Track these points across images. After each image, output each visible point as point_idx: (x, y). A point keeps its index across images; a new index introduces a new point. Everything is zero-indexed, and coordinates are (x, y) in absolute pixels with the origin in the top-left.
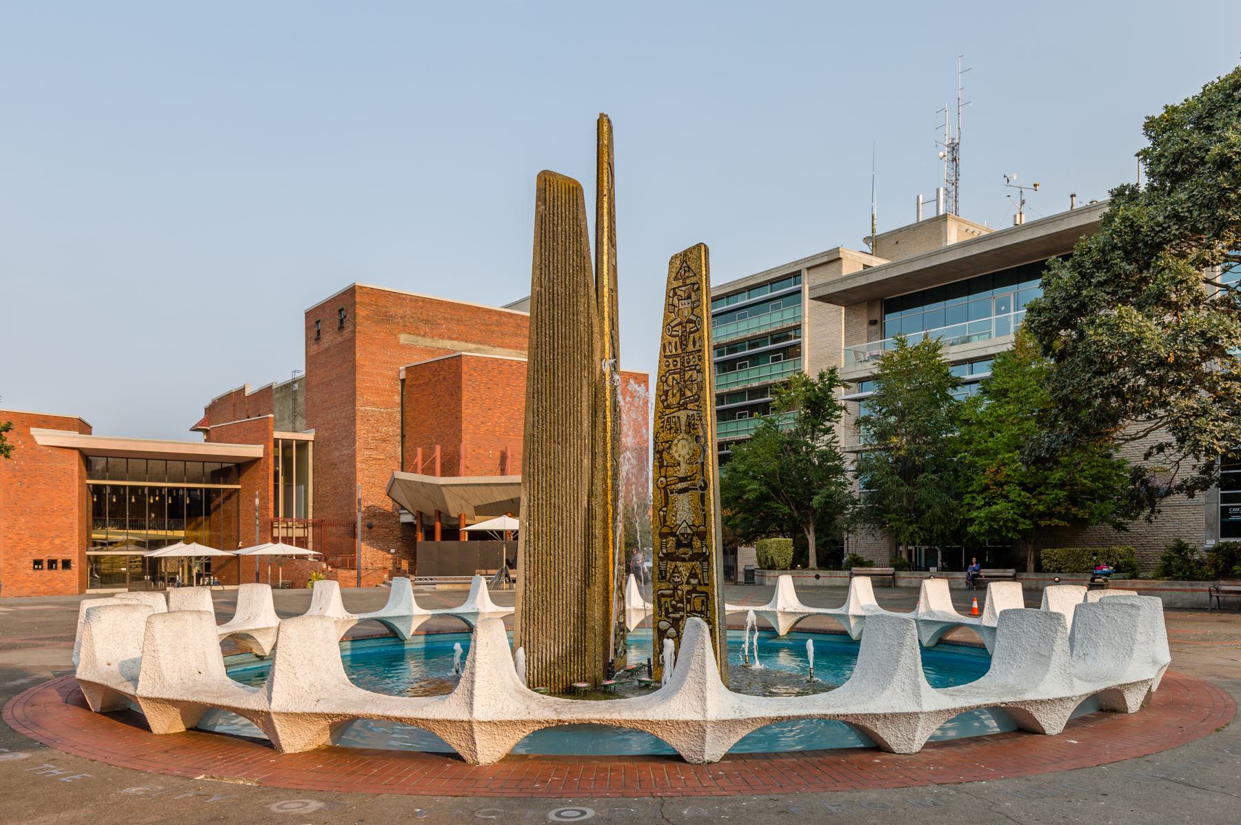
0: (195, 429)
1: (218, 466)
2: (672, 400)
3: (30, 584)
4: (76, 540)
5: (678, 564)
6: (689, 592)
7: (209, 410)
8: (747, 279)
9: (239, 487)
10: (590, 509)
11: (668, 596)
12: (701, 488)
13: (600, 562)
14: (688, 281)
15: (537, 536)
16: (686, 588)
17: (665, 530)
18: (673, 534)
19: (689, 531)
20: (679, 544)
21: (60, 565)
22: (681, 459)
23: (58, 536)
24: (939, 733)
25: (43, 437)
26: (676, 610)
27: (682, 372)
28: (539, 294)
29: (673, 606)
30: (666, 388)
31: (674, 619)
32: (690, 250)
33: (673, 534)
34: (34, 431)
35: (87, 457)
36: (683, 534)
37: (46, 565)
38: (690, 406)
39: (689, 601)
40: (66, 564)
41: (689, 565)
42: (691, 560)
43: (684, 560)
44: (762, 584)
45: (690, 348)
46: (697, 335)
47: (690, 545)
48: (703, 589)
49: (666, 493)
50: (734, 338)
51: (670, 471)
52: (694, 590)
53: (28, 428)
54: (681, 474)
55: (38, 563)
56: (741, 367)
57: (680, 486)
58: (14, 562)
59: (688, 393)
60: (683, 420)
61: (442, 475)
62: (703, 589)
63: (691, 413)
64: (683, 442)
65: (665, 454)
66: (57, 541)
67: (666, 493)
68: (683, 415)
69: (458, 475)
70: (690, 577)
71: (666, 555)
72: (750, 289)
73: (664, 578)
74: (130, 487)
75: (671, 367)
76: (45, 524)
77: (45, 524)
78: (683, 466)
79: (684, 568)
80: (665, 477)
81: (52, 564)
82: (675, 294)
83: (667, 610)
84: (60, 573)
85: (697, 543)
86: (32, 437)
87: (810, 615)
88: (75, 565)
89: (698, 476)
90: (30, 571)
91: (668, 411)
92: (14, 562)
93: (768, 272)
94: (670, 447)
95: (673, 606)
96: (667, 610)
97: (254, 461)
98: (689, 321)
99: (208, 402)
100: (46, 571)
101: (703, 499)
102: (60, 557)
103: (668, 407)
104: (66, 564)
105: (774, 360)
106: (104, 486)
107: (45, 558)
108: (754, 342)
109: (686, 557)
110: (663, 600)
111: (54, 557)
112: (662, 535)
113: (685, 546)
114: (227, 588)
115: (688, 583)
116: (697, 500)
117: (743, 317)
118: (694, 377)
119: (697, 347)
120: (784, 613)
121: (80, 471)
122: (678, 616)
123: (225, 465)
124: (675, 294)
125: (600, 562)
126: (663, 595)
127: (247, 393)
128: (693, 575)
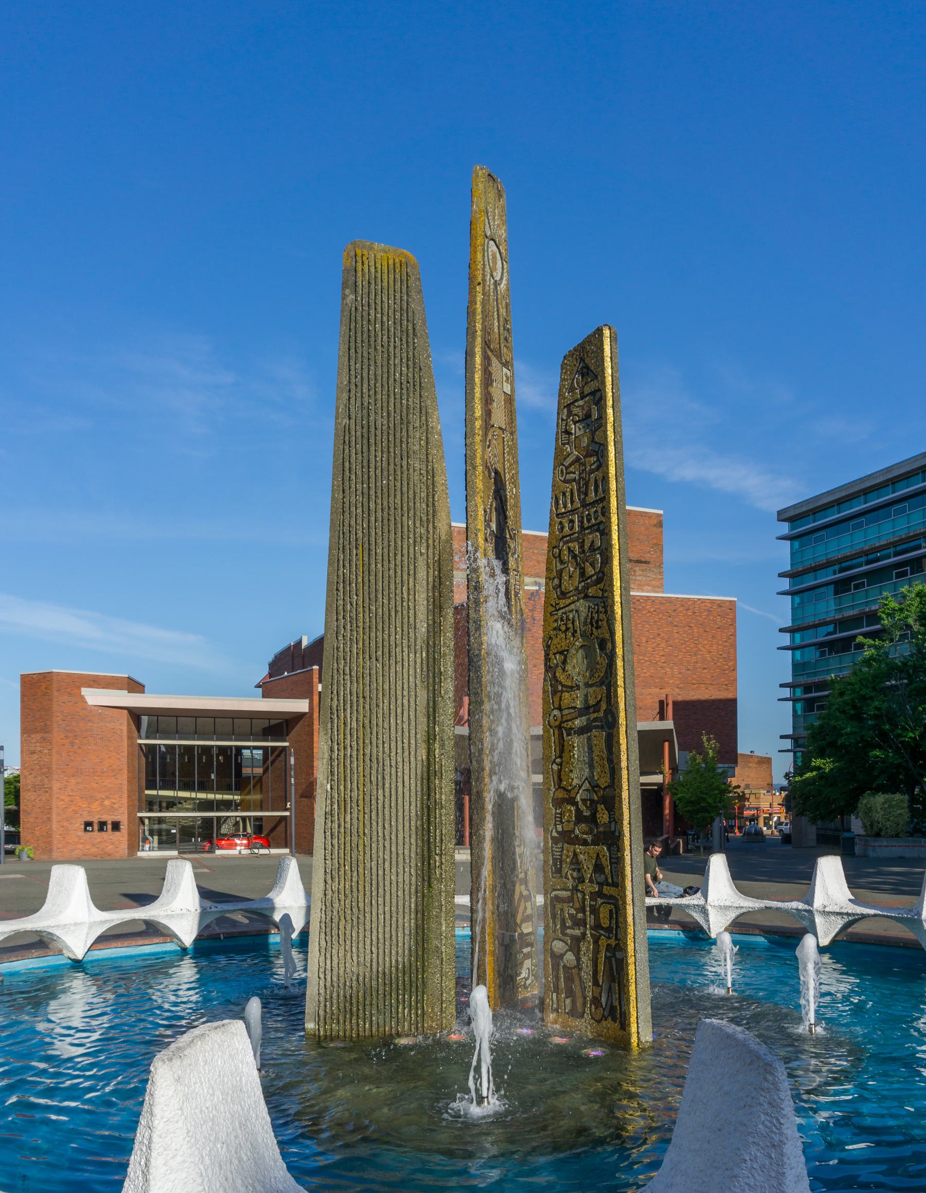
0: (256, 687)
1: (266, 723)
2: (569, 585)
3: (81, 846)
4: (125, 801)
5: (579, 848)
7: (272, 665)
8: (862, 480)
9: (286, 744)
15: (343, 804)
21: (110, 827)
23: (107, 797)
25: (94, 697)
28: (347, 430)
31: (573, 937)
34: (85, 691)
35: (135, 715)
37: (96, 827)
40: (116, 826)
41: (592, 849)
42: (595, 843)
44: (865, 856)
45: (592, 496)
46: (599, 474)
49: (561, 735)
50: (847, 552)
53: (79, 688)
55: (88, 824)
56: (857, 587)
58: (66, 824)
59: (590, 571)
66: (107, 803)
67: (561, 735)
72: (866, 492)
74: (219, 747)
76: (95, 785)
77: (95, 785)
80: (560, 709)
81: (102, 825)
84: (109, 835)
86: (83, 698)
87: (864, 917)
88: (124, 827)
89: (604, 706)
90: (81, 833)
91: (562, 603)
92: (66, 824)
93: (889, 469)
94: (564, 662)
97: (298, 717)
99: (271, 658)
100: (96, 833)
102: (109, 818)
103: (564, 595)
104: (116, 826)
105: (899, 575)
106: (212, 747)
107: (95, 820)
108: (869, 554)
111: (104, 818)
112: (558, 803)
114: (274, 851)
117: (860, 525)
120: (825, 913)
121: (129, 731)
123: (273, 722)
124: (570, 413)
127: (305, 643)
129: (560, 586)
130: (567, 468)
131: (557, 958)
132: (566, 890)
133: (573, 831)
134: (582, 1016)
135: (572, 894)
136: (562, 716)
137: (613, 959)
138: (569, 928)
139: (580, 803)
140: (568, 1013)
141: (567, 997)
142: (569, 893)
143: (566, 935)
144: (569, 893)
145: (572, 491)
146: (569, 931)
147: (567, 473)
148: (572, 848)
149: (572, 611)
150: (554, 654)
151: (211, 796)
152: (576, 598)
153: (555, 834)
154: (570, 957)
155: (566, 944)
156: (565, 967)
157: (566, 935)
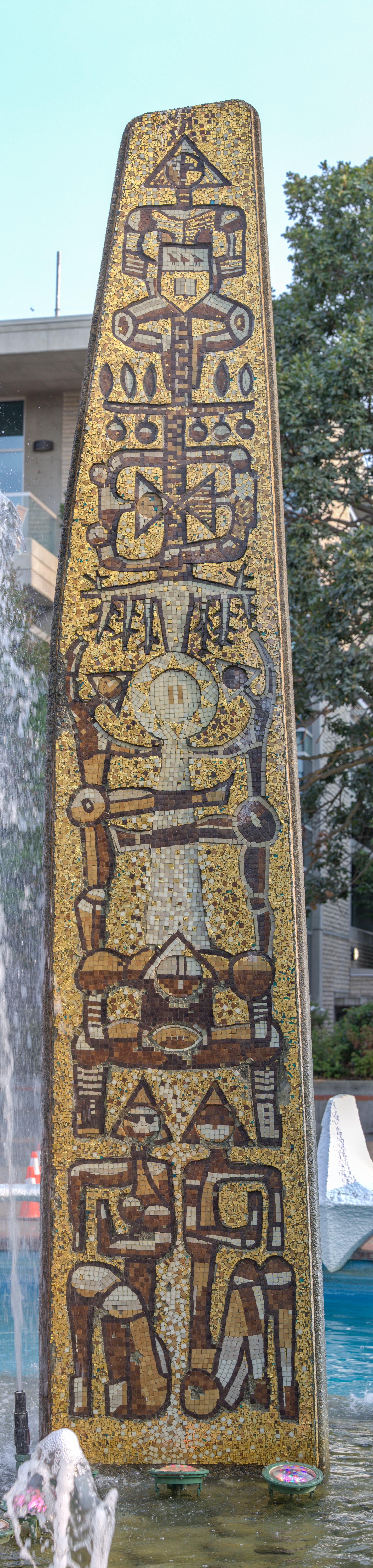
5: (153, 1075)
6: (193, 1168)
11: (106, 1182)
12: (248, 831)
13: (247, 1176)
14: (199, 197)
16: (182, 1154)
17: (99, 963)
18: (137, 980)
19: (193, 969)
20: (154, 1012)
22: (164, 733)
24: (294, 1082)
26: (141, 1226)
27: (176, 458)
29: (128, 1215)
30: (110, 503)
31: (132, 1257)
32: (213, 111)
33: (137, 980)
36: (168, 980)
38: (205, 570)
39: (193, 1197)
41: (199, 1079)
43: (174, 1063)
45: (207, 392)
47: (202, 1014)
48: (258, 1155)
51: (123, 771)
52: (217, 1159)
54: (168, 778)
57: (160, 820)
59: (197, 529)
60: (176, 611)
62: (258, 1155)
63: (205, 592)
64: (176, 680)
65: (103, 713)
67: (105, 845)
68: (175, 597)
70: (198, 1118)
71: (104, 1047)
73: (100, 1121)
75: (132, 440)
78: (173, 754)
79: (179, 1092)
80: (104, 788)
82: (148, 225)
83: (107, 1229)
85: (230, 1009)
89: (241, 793)
91: (115, 577)
94: (123, 690)
95: (128, 1215)
96: (107, 1229)
98: (200, 311)
101: (255, 869)
103: (119, 562)
109: (185, 1053)
110: (93, 1195)
113: (179, 1016)
115: (191, 1137)
116: (235, 872)
118: (223, 483)
119: (234, 394)
122: (146, 1245)
124: (148, 225)
125: (247, 1176)
126: (88, 1180)
128: (215, 1109)
129: (112, 540)
130: (137, 321)
131: (84, 1306)
132: (115, 1161)
133: (139, 1039)
134: (267, 1407)
135: (133, 1168)
136: (108, 803)
137: (257, 1291)
138: (122, 1237)
139: (157, 984)
140: (115, 1415)
141: (113, 1381)
142: (123, 1167)
143: (111, 1253)
144: (123, 1167)
145: (151, 368)
146: (121, 1245)
147: (136, 331)
148: (135, 1075)
149: (143, 598)
150: (90, 676)
151: (321, 1289)
152: (153, 575)
153: (82, 1045)
154: (125, 1300)
155: (116, 1271)
156: (108, 1320)
157: (111, 1253)
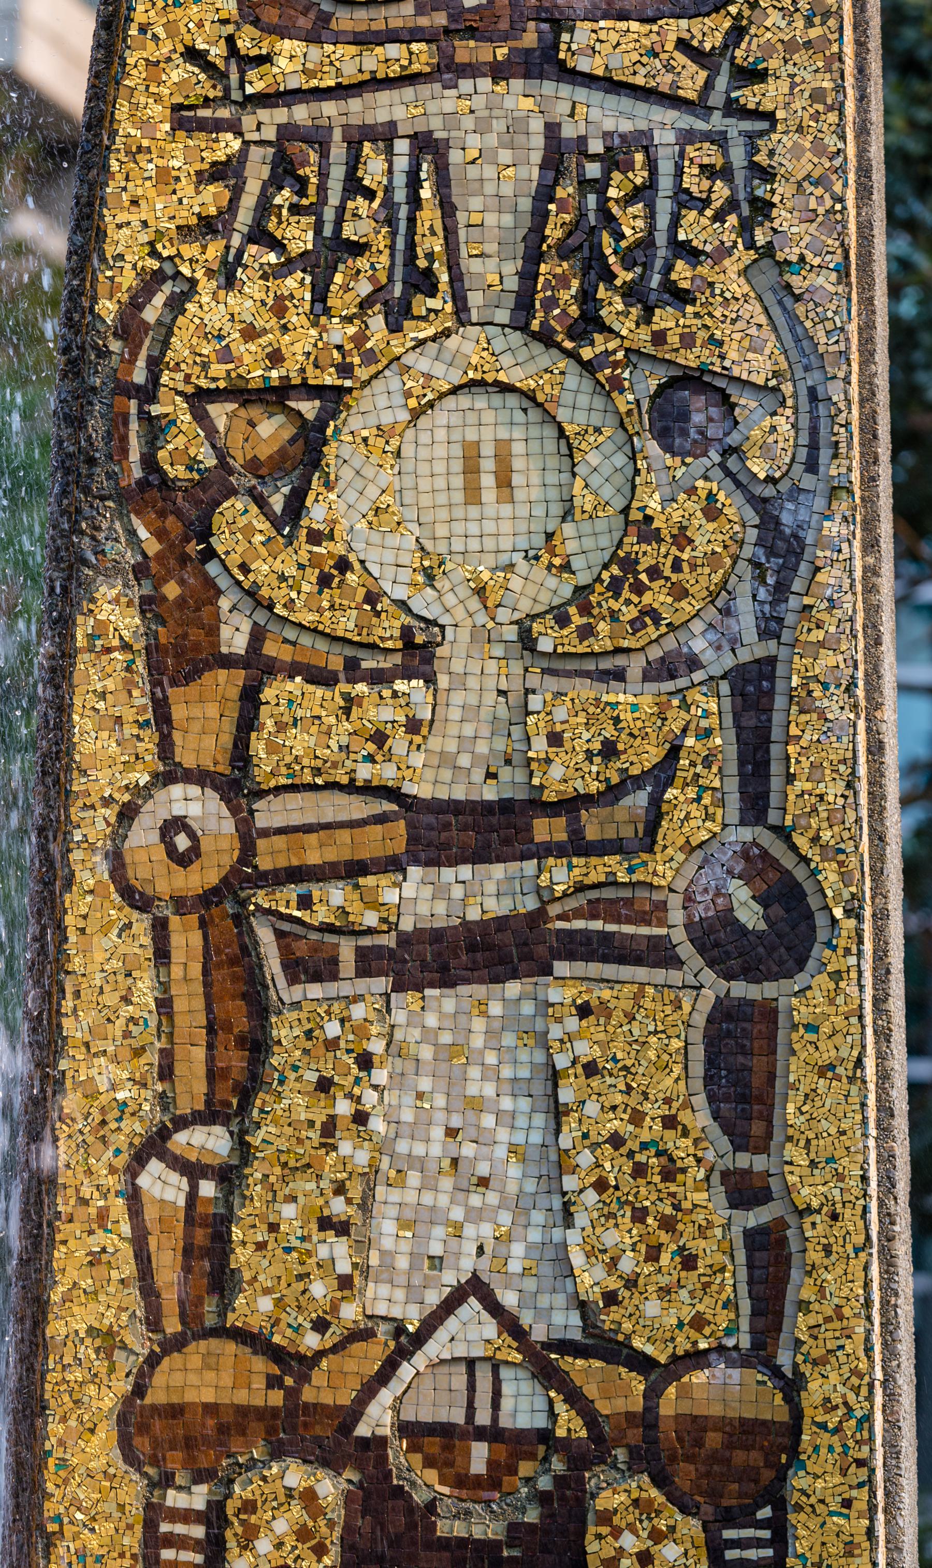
10: (867, 1339)
12: (720, 942)
17: (205, 1378)
18: (330, 1438)
22: (445, 604)
33: (330, 1438)
36: (437, 1441)
54: (452, 759)
57: (423, 898)
60: (496, 181)
61: (887, 149)
63: (601, 118)
64: (490, 423)
65: (239, 528)
69: (889, 235)
78: (475, 677)
80: (236, 783)
89: (700, 815)
94: (307, 453)
101: (741, 1071)
116: (672, 1074)
